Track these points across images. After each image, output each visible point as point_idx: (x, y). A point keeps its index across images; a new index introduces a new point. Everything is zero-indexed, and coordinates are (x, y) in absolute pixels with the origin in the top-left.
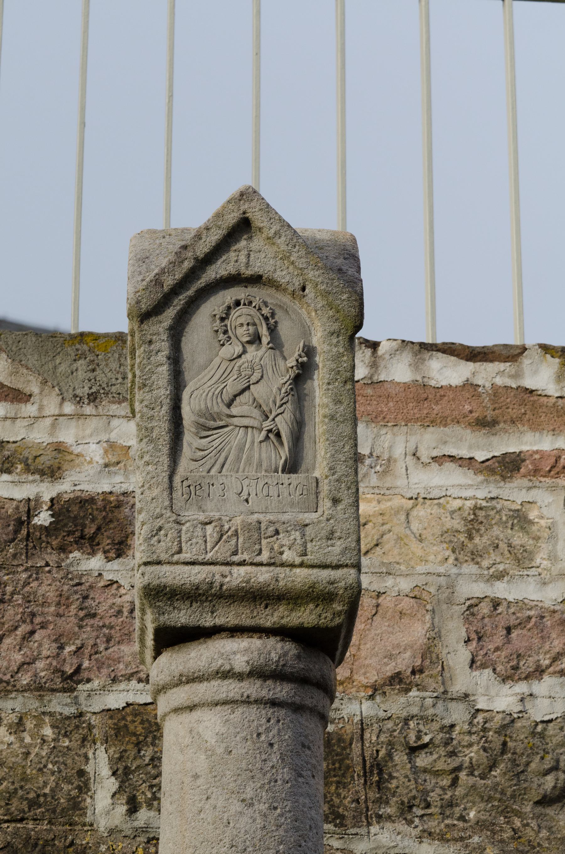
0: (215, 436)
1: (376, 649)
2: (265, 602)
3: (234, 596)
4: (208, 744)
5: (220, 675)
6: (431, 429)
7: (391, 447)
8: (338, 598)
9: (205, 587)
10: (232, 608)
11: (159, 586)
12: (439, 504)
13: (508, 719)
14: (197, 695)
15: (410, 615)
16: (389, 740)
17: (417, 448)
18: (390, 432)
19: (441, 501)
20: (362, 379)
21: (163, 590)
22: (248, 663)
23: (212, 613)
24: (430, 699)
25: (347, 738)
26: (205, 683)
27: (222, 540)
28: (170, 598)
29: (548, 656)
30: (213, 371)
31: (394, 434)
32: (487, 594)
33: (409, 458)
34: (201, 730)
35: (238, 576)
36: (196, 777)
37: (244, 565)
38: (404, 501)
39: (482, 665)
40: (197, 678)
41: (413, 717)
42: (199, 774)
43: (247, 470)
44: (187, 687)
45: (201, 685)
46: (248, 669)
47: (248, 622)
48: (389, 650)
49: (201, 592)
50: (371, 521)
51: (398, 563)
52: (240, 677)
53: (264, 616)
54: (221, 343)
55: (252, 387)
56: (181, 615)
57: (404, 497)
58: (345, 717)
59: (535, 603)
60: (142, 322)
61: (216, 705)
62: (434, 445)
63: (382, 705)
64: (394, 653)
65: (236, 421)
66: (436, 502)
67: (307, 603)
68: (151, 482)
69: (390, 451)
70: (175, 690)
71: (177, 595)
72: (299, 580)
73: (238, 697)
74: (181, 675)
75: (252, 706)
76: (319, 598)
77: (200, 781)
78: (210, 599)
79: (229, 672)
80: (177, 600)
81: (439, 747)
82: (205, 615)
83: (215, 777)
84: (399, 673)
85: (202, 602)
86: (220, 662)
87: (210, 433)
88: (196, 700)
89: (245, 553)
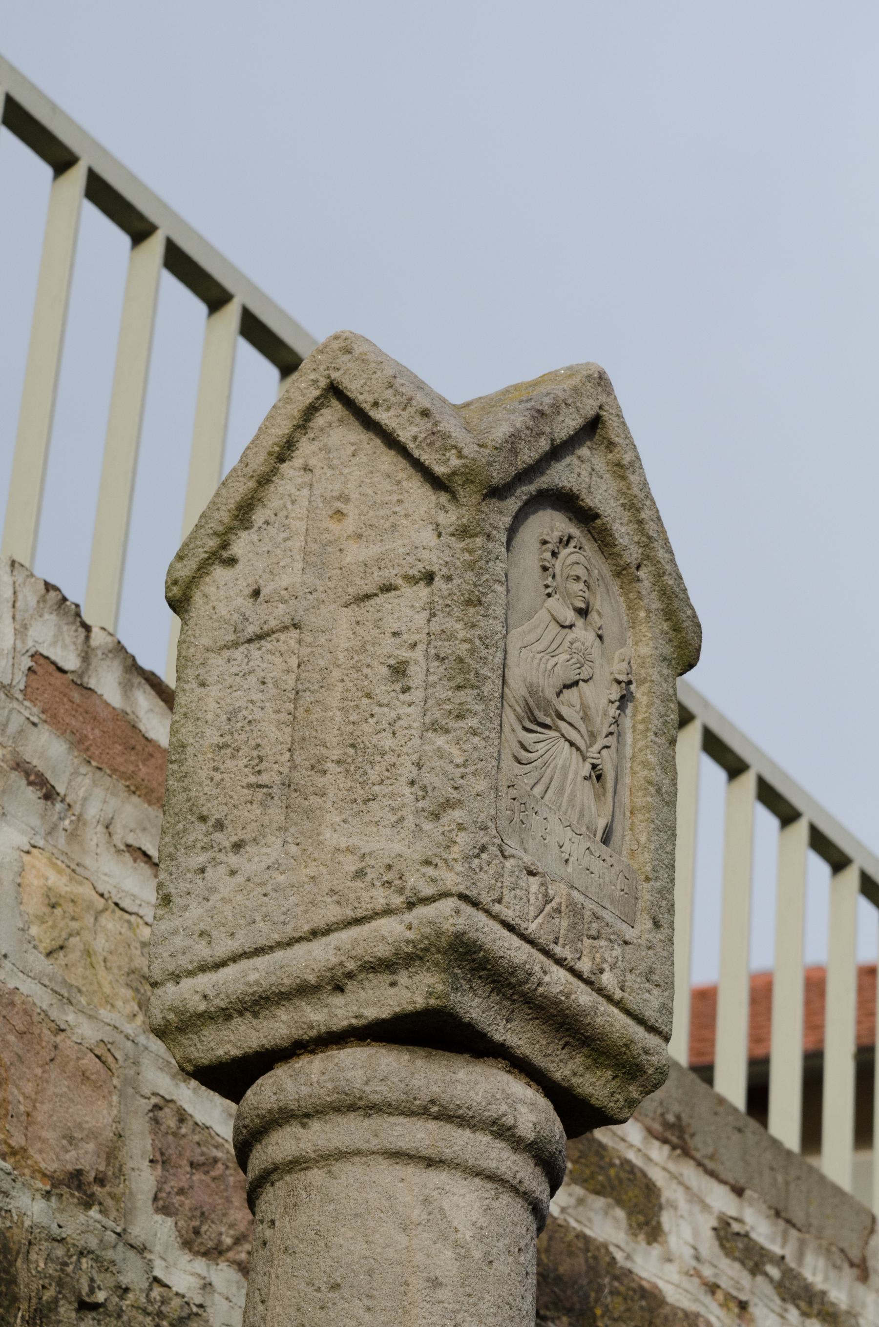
0: (542, 737)
1: (55, 1118)
2: (567, 1039)
3: (543, 1009)
4: (459, 1236)
5: (495, 1128)
6: (135, 799)
7: (85, 799)
8: (642, 1079)
9: (522, 976)
10: (529, 1027)
11: (475, 942)
12: (129, 922)
13: (186, 1311)
14: (451, 1147)
15: (95, 1082)
16: (60, 1277)
17: (112, 818)
18: (90, 775)
19: (133, 918)
20: (73, 672)
21: (475, 952)
22: (535, 1127)
23: (508, 1021)
24: (112, 1234)
25: (15, 1247)
26: (468, 1132)
27: (544, 913)
28: (474, 969)
29: (232, 1232)
30: (539, 631)
31: (94, 781)
32: (174, 1098)
33: (100, 828)
34: (447, 1207)
35: (556, 981)
36: (435, 1283)
37: (562, 966)
38: (94, 893)
39: (163, 1207)
40: (458, 1117)
41: (89, 1252)
42: (440, 1279)
43: (569, 812)
44: (432, 1125)
45: (460, 1131)
46: (531, 1136)
47: (538, 1060)
48: (69, 1128)
49: (513, 980)
50: (60, 905)
51: (80, 991)
52: (517, 1143)
53: (557, 1059)
54: (549, 590)
55: (581, 683)
56: (474, 1004)
57: (95, 888)
58: (13, 1211)
59: (220, 1140)
60: (485, 497)
61: (477, 1175)
62: (132, 825)
63: (57, 1215)
64: (76, 1135)
65: (562, 725)
66: (127, 916)
67: (607, 1067)
68: (479, 766)
69: (83, 805)
70: (401, 1119)
71: (485, 969)
72: (618, 1026)
73: (509, 1176)
74: (432, 1102)
75: (517, 1199)
76: (624, 1067)
77: (440, 1294)
78: (516, 997)
79: (509, 1129)
80: (480, 977)
81: (110, 1316)
82: (498, 1021)
83: (469, 1295)
84: (79, 1172)
85: (505, 997)
86: (504, 1108)
87: (539, 729)
88: (448, 1153)
89: (567, 947)
